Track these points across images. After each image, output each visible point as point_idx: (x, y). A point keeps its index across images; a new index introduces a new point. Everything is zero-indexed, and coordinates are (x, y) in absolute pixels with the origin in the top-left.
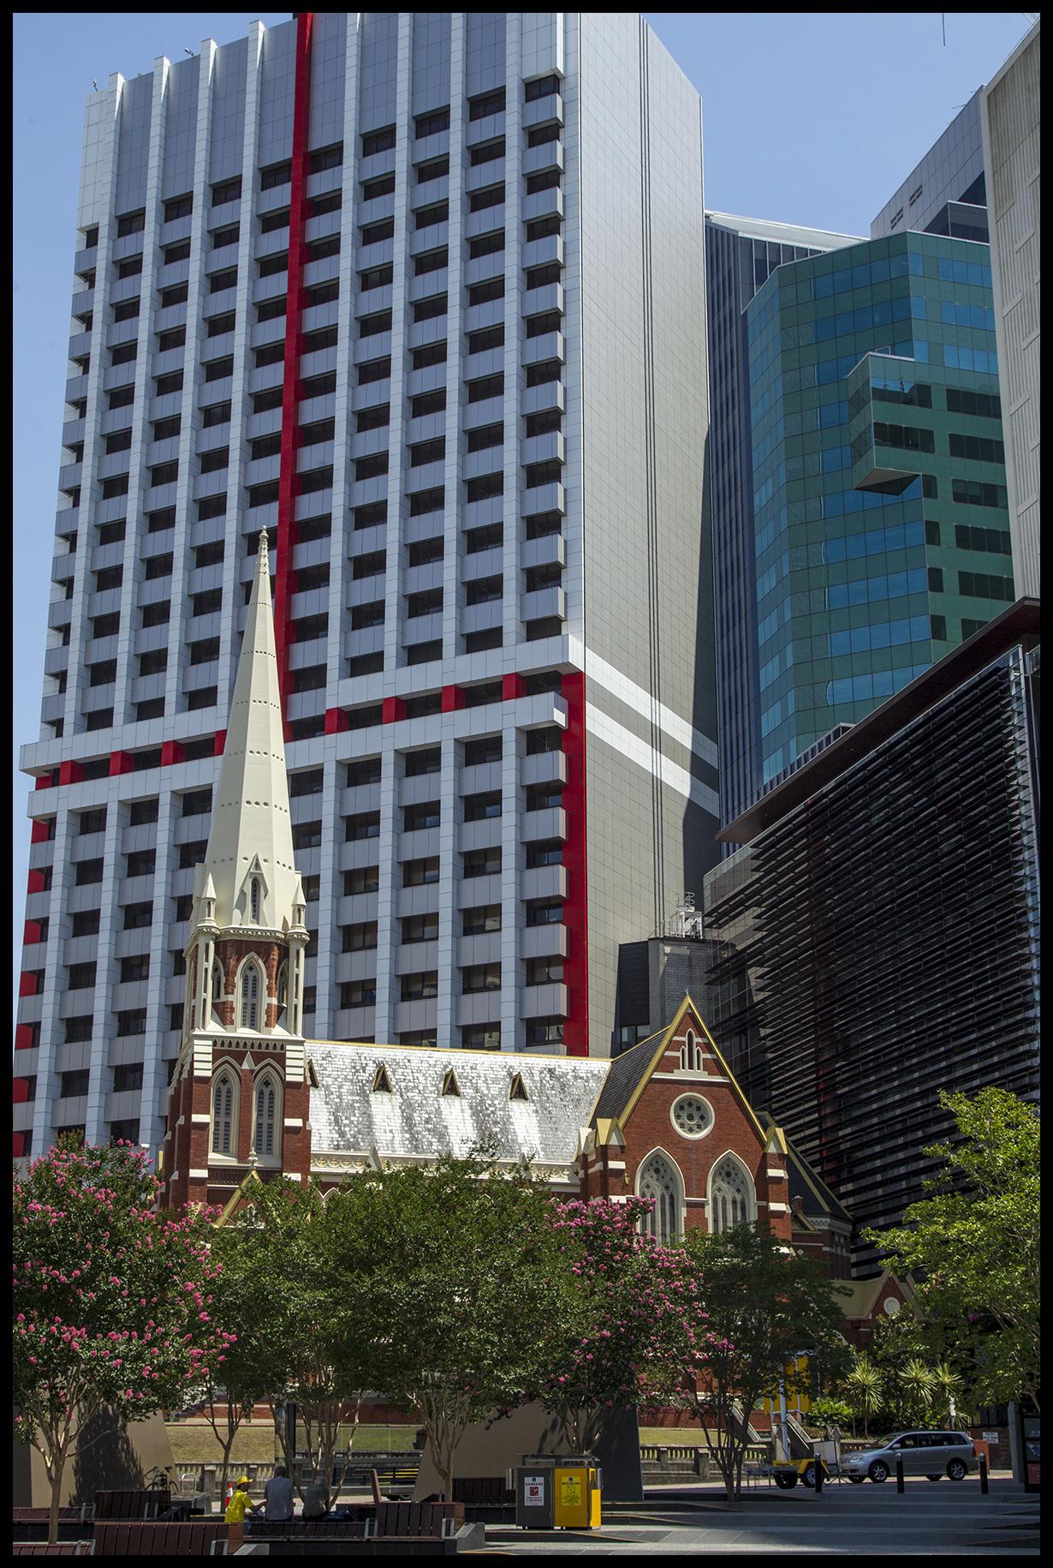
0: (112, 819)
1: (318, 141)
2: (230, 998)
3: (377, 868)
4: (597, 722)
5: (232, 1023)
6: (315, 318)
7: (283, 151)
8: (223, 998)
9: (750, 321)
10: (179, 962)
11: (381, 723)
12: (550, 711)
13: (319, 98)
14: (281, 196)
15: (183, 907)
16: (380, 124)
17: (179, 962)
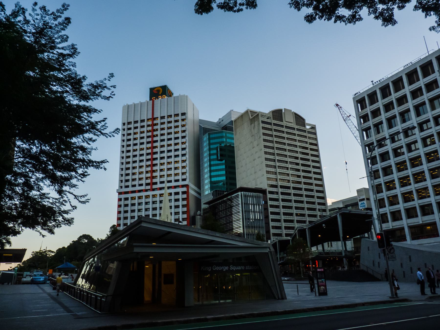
12: (185, 189)
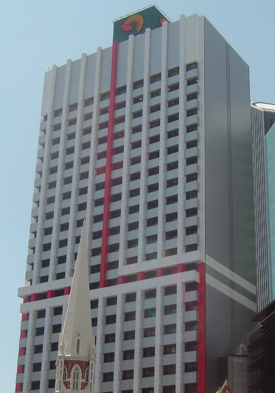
0: (47, 314)
1: (119, 85)
2: (69, 380)
3: (176, 324)
4: (210, 280)
5: (69, 388)
6: (117, 143)
7: (107, 88)
8: (67, 380)
9: (267, 139)
10: (52, 365)
11: (176, 273)
12: (192, 276)
13: (120, 70)
14: (106, 103)
15: (54, 347)
16: (139, 79)
17: (52, 365)
